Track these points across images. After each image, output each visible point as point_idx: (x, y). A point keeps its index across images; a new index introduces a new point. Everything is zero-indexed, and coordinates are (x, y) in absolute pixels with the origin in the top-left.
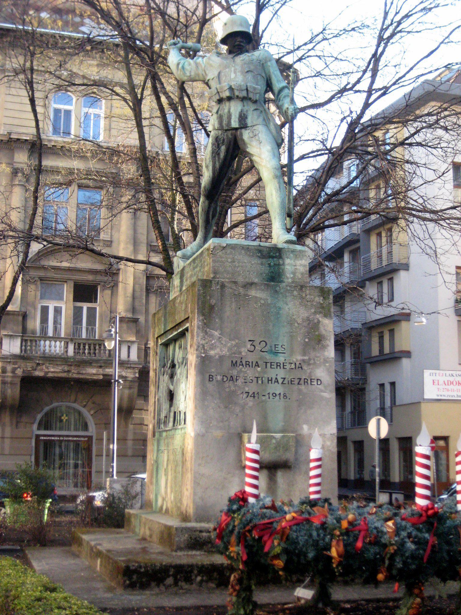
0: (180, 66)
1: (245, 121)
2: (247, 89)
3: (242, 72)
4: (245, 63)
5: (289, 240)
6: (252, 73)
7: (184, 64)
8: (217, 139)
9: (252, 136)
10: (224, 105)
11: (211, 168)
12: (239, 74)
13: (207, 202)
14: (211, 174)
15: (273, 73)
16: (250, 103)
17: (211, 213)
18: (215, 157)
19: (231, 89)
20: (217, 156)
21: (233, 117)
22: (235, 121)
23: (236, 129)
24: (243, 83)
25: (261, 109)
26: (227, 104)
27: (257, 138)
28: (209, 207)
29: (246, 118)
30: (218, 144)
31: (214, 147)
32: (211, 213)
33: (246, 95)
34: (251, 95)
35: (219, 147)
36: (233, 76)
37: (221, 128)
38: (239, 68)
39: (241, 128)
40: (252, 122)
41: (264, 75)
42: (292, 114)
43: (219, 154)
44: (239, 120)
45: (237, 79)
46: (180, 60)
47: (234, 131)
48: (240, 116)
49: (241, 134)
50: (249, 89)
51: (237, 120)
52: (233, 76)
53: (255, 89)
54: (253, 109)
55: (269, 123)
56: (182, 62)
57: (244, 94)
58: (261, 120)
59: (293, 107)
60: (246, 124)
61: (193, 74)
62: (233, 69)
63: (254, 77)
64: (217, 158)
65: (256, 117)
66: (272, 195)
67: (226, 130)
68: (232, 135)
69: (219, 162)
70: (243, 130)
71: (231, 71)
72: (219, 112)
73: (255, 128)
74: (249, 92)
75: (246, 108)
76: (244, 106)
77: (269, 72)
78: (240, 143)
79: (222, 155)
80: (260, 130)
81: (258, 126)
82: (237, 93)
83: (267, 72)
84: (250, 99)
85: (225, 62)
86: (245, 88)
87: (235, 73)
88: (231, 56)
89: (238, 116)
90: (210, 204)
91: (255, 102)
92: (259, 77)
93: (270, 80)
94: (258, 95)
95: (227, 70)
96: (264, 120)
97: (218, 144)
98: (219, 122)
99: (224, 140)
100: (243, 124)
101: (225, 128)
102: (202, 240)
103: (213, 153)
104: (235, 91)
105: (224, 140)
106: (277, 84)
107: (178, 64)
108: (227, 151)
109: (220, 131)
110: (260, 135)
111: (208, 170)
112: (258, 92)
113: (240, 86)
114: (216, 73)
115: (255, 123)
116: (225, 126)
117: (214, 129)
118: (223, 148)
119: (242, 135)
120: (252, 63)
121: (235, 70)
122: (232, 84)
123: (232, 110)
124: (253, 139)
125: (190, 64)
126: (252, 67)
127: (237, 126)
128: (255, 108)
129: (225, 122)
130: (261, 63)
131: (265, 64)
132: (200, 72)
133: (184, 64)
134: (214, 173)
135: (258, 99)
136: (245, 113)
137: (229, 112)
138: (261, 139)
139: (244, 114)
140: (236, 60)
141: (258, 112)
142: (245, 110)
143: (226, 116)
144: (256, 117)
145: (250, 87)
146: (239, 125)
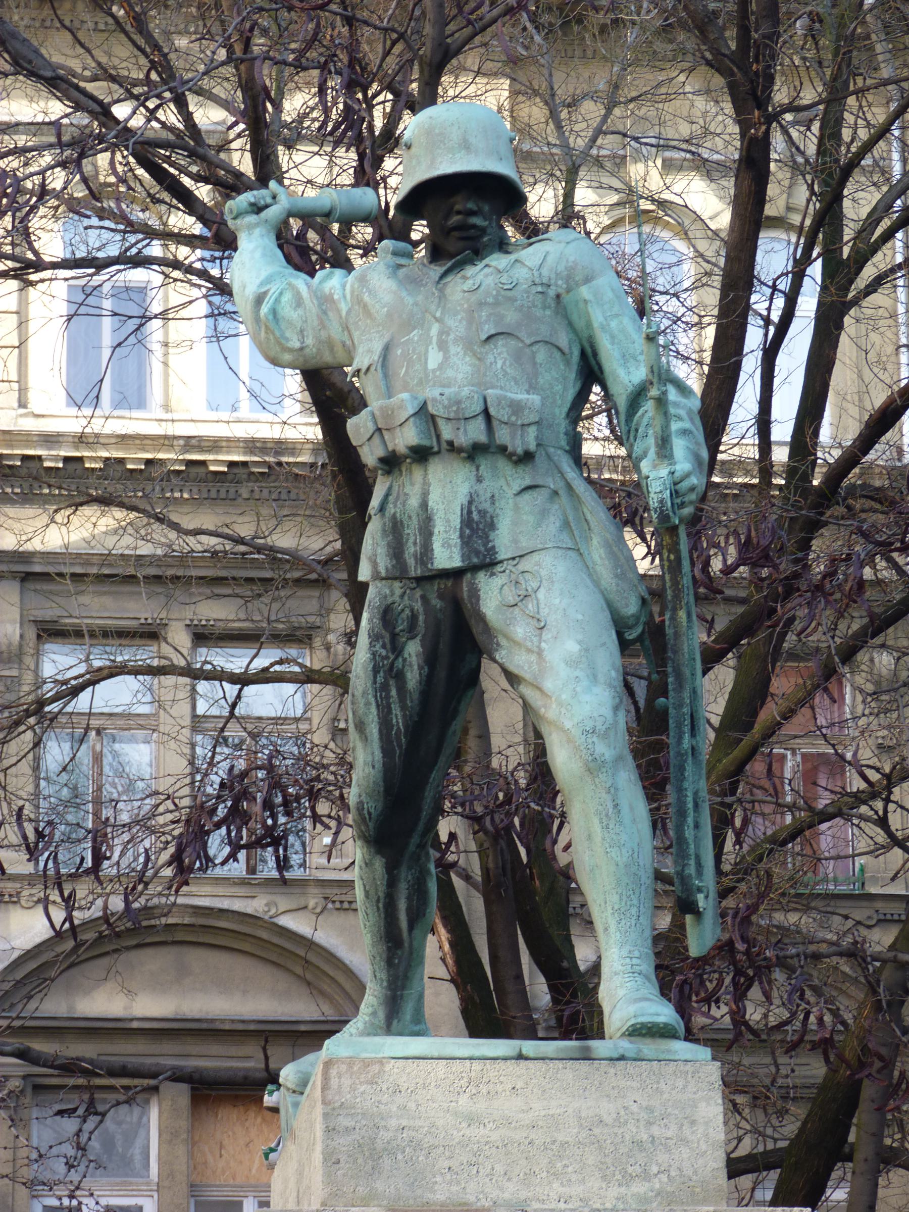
0: (265, 309)
1: (486, 539)
2: (486, 412)
3: (468, 345)
4: (481, 304)
5: (643, 1025)
6: (513, 342)
7: (277, 301)
8: (387, 615)
9: (511, 600)
10: (404, 478)
11: (373, 730)
12: (455, 350)
13: (379, 864)
14: (378, 755)
15: (603, 328)
16: (503, 464)
17: (402, 905)
18: (385, 687)
19: (423, 412)
20: (392, 682)
21: (439, 528)
22: (446, 545)
23: (456, 574)
24: (466, 391)
25: (552, 483)
26: (418, 473)
27: (531, 607)
28: (392, 883)
29: (492, 526)
30: (394, 637)
31: (378, 647)
32: (402, 905)
33: (483, 438)
34: (503, 436)
35: (396, 649)
36: (434, 359)
37: (398, 573)
38: (457, 325)
39: (475, 569)
40: (515, 541)
41: (563, 339)
42: (661, 502)
43: (400, 677)
44: (461, 536)
45: (450, 373)
46: (269, 280)
47: (450, 583)
48: (467, 521)
49: (475, 594)
50: (492, 411)
51: (455, 538)
52: (434, 359)
53: (517, 408)
54: (516, 486)
55: (588, 539)
56: (274, 289)
57: (476, 432)
58: (553, 525)
59: (664, 472)
60: (492, 551)
61: (309, 341)
62: (435, 329)
63: (517, 357)
64: (394, 692)
65: (530, 519)
66: (589, 837)
67: (419, 580)
68: (441, 596)
69: (403, 708)
70: (481, 576)
71: (427, 341)
72: (391, 509)
73: (525, 565)
74: (495, 423)
75: (489, 486)
76: (479, 480)
77: (589, 325)
78: (477, 630)
79: (413, 678)
80: (543, 573)
81: (536, 557)
82: (447, 433)
83: (580, 324)
84: (503, 449)
85: (409, 300)
86: (478, 408)
87: (442, 346)
88: (437, 270)
89: (456, 522)
90: (392, 869)
91: (527, 457)
92: (542, 354)
93: (595, 354)
94: (532, 432)
95: (415, 334)
96: (566, 525)
97: (394, 637)
98: (389, 545)
99: (414, 617)
100: (477, 553)
101: (415, 570)
102: (381, 1015)
103: (376, 671)
104: (441, 424)
105: (414, 617)
106: (621, 372)
107: (259, 300)
108: (431, 659)
109: (397, 584)
110: (541, 595)
111: (365, 738)
112: (533, 418)
113: (458, 402)
114: (377, 347)
115: (526, 544)
116: (411, 562)
117: (376, 576)
118: (413, 649)
119: (478, 598)
120: (513, 300)
121: (444, 332)
122: (431, 393)
123: (435, 501)
124: (516, 610)
125: (299, 302)
126: (511, 317)
127: (456, 562)
128: (528, 482)
129: (411, 550)
130: (552, 292)
131: (566, 298)
132: (335, 332)
133: (277, 301)
134: (387, 751)
135: (532, 447)
136: (486, 506)
137: (424, 505)
138: (544, 612)
139: (482, 513)
140: (448, 291)
141: (539, 497)
142: (485, 496)
143: (415, 521)
144: (531, 519)
145: (499, 399)
146: (464, 557)
